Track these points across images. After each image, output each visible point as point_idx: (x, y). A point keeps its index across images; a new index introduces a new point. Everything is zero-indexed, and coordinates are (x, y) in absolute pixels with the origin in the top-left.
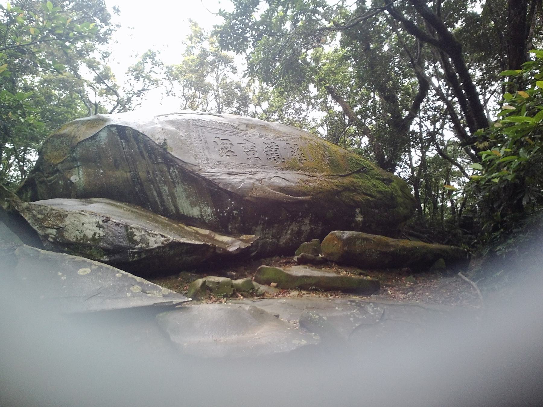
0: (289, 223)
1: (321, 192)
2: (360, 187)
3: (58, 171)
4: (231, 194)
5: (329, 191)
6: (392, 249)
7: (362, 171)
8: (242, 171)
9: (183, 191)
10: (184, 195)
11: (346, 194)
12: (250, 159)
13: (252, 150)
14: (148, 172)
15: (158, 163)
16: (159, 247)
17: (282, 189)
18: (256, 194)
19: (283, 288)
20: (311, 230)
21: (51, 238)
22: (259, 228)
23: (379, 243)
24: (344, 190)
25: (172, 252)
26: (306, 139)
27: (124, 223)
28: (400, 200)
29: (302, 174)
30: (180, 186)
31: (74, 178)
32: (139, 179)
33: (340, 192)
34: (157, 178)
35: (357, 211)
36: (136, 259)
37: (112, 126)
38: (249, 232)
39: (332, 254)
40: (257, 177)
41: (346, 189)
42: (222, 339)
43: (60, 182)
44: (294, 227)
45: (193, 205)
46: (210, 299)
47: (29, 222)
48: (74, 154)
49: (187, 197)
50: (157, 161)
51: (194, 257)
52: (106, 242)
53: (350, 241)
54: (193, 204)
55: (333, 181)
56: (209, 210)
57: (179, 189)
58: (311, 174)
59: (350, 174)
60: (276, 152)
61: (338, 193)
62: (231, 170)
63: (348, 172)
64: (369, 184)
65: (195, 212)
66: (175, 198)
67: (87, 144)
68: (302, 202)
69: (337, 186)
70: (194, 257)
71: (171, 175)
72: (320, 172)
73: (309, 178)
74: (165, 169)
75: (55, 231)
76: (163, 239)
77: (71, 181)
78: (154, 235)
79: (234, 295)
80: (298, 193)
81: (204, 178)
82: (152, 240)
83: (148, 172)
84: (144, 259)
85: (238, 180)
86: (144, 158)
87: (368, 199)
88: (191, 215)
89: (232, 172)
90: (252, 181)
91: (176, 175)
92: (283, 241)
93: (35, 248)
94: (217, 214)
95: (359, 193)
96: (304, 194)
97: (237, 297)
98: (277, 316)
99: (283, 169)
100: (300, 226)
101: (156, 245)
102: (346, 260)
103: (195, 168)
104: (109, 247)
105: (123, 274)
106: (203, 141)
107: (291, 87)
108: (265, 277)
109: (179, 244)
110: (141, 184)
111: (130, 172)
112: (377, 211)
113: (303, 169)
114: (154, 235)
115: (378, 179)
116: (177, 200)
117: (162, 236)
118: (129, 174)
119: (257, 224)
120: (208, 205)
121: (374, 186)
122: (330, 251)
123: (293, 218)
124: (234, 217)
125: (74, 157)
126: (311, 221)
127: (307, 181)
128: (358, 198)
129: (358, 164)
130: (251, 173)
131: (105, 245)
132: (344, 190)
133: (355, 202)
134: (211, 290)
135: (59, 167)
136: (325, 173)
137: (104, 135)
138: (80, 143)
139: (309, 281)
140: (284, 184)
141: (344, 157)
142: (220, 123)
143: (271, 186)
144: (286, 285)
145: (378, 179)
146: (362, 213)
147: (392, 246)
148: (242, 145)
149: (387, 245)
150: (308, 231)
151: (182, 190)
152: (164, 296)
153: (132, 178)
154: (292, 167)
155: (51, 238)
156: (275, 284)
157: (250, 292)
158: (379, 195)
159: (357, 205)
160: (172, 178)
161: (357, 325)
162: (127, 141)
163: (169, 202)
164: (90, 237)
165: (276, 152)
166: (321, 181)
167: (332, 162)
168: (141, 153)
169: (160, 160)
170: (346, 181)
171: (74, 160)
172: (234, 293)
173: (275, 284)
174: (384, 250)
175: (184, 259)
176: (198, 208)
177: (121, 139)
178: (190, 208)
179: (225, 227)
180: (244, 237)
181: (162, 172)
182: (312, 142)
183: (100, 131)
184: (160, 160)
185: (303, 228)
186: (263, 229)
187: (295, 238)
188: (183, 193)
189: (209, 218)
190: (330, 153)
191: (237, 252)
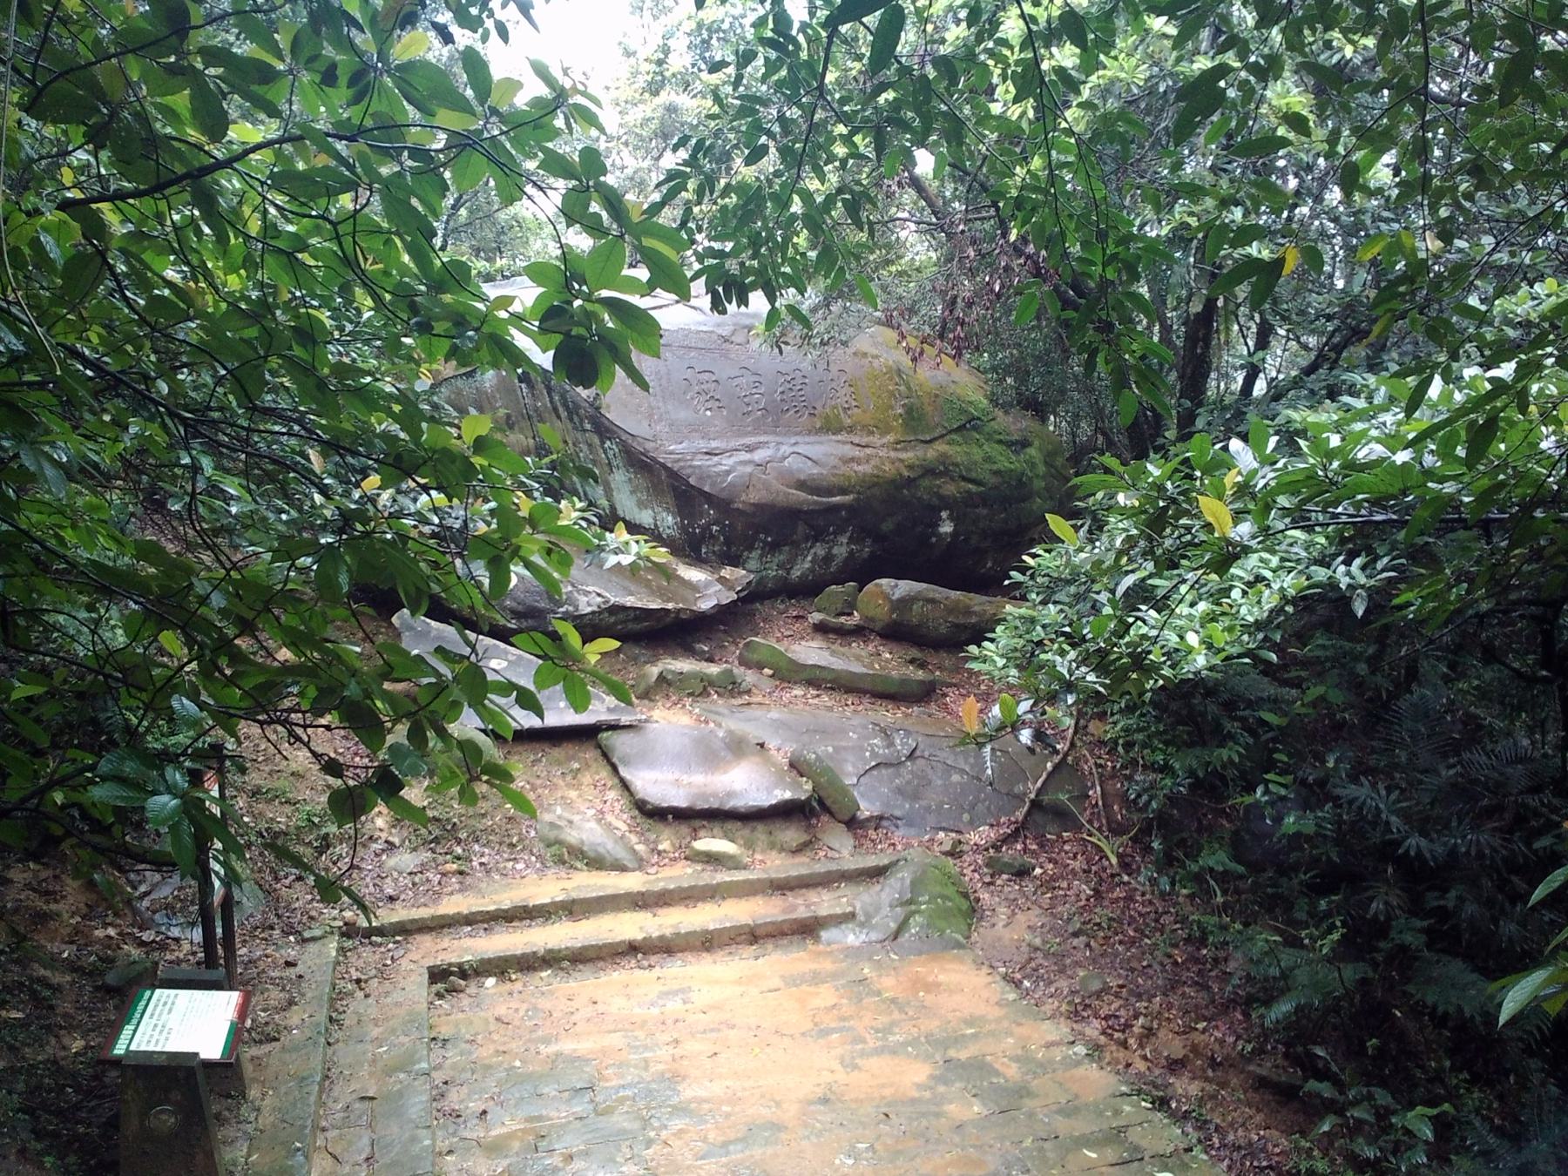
1: (875, 485)
2: (957, 465)
4: (708, 497)
5: (893, 481)
6: (974, 620)
7: (969, 425)
8: (734, 444)
10: (627, 488)
11: (925, 482)
12: (749, 413)
15: (585, 431)
16: (593, 613)
17: (802, 485)
18: (754, 497)
19: (782, 680)
20: (851, 553)
22: (755, 554)
23: (953, 609)
24: (922, 476)
25: (612, 620)
26: (865, 355)
28: (1039, 484)
29: (844, 443)
33: (915, 479)
35: (944, 514)
38: (735, 562)
39: (872, 620)
40: (759, 455)
41: (929, 471)
42: (685, 779)
44: (820, 550)
46: (668, 697)
49: (632, 492)
52: (514, 599)
53: (905, 603)
54: (642, 505)
55: (903, 455)
58: (865, 440)
59: (942, 436)
61: (910, 482)
62: (714, 444)
63: (939, 431)
64: (977, 454)
68: (836, 508)
69: (910, 467)
71: (605, 452)
72: (883, 434)
73: (857, 452)
74: (596, 440)
76: (599, 599)
78: (587, 593)
79: (704, 693)
80: (830, 492)
81: (663, 466)
82: (583, 600)
86: (559, 417)
87: (968, 492)
90: (749, 469)
92: (796, 573)
94: (683, 528)
95: (952, 479)
96: (843, 491)
97: (709, 695)
98: (762, 745)
99: (810, 433)
100: (830, 548)
101: (589, 609)
102: (896, 632)
103: (649, 446)
104: (520, 608)
106: (664, 382)
108: (755, 657)
109: (624, 608)
112: (985, 512)
113: (851, 430)
114: (587, 593)
115: (1000, 442)
119: (751, 548)
120: (667, 510)
121: (988, 459)
122: (871, 614)
123: (818, 536)
124: (712, 536)
126: (850, 538)
127: (852, 460)
128: (950, 489)
129: (963, 411)
131: (514, 604)
132: (922, 476)
133: (941, 498)
134: (669, 684)
136: (890, 438)
139: (825, 674)
140: (810, 471)
141: (937, 396)
142: (698, 332)
143: (783, 475)
144: (790, 674)
145: (1000, 442)
146: (951, 518)
147: (975, 613)
148: (736, 382)
154: (831, 426)
156: (770, 672)
157: (730, 687)
158: (993, 480)
159: (946, 502)
162: (531, 386)
166: (875, 456)
167: (909, 410)
168: (555, 409)
169: (588, 427)
170: (931, 453)
172: (702, 689)
173: (770, 672)
174: (961, 620)
177: (521, 381)
178: (636, 510)
179: (697, 550)
180: (727, 572)
181: (590, 445)
182: (876, 363)
185: (835, 551)
186: (761, 556)
190: (909, 388)
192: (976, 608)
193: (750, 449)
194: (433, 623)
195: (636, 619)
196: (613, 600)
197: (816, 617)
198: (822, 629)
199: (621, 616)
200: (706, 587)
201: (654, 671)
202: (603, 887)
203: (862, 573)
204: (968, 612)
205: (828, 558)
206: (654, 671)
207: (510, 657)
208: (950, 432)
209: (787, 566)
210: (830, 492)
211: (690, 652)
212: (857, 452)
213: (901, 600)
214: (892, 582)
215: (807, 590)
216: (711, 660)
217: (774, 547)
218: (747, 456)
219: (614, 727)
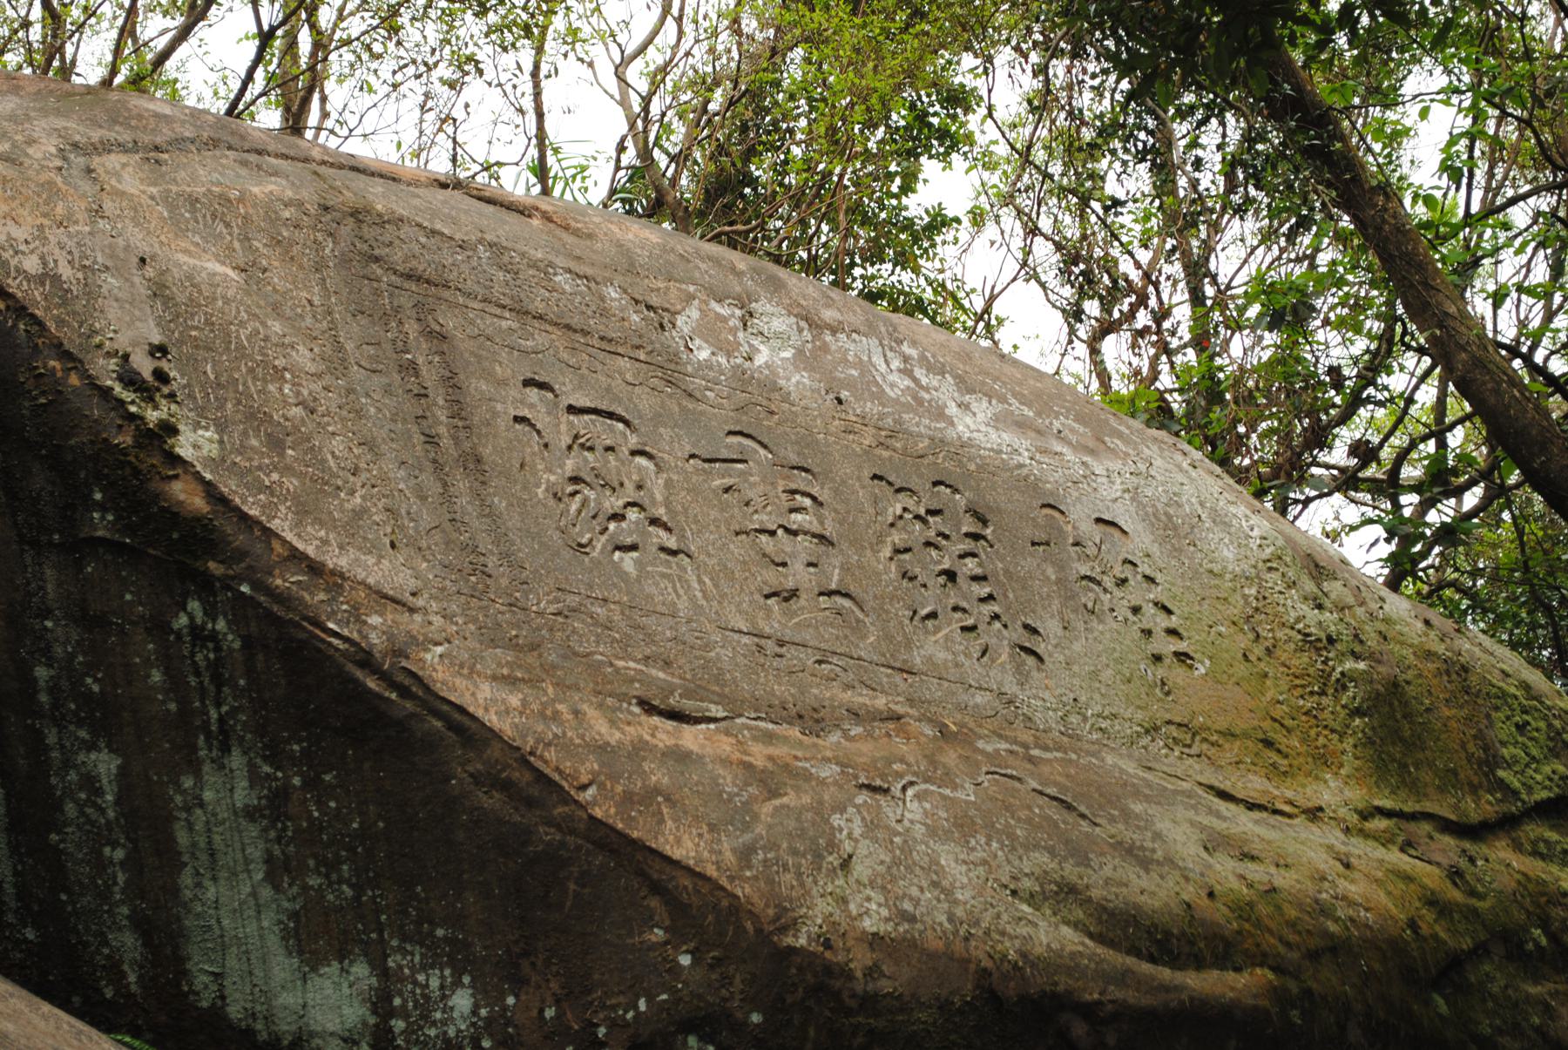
9: (251, 814)
10: (254, 844)
15: (79, 548)
27: (1037, 871)
30: (236, 760)
34: (42, 673)
45: (316, 938)
49: (277, 870)
56: (462, 1001)
57: (224, 790)
61: (1451, 970)
66: (170, 859)
88: (286, 1027)
91: (215, 668)
96: (404, 692)
107: (1249, 200)
116: (186, 878)
149: (1178, 988)
151: (242, 795)
160: (175, 683)
163: (104, 895)
176: (360, 970)
178: (282, 966)
188: (253, 831)
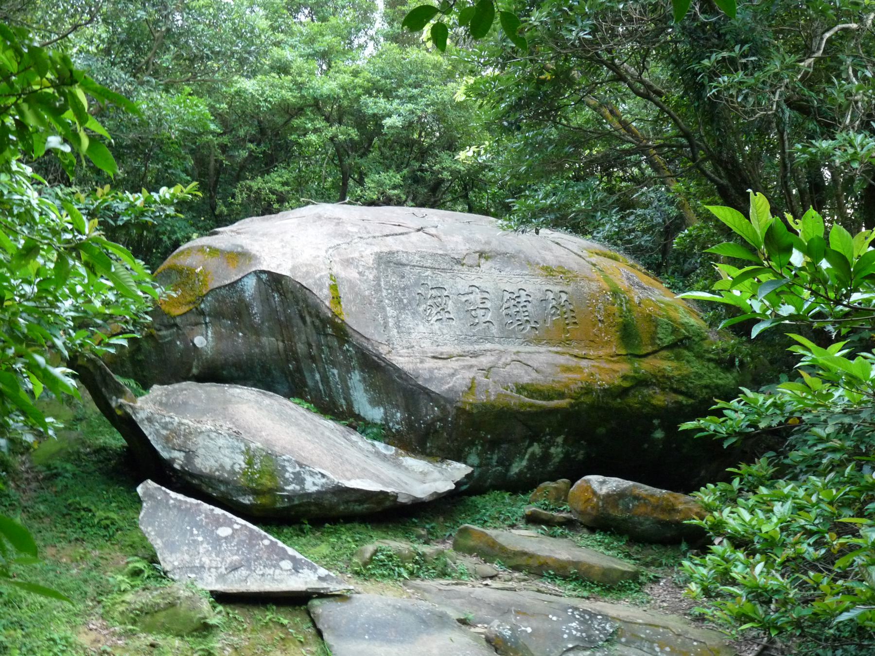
0: (527, 443)
3: (176, 325)
13: (482, 306)
14: (310, 346)
15: (326, 335)
16: (318, 492)
17: (521, 389)
21: (179, 464)
29: (563, 354)
31: (199, 341)
32: (295, 353)
36: (286, 505)
37: (264, 272)
40: (485, 361)
41: (642, 382)
43: (178, 343)
47: (149, 438)
48: (203, 306)
50: (324, 331)
51: (366, 506)
56: (399, 415)
57: (356, 377)
60: (525, 309)
62: (477, 347)
65: (376, 414)
67: (224, 292)
69: (625, 378)
70: (366, 506)
73: (573, 362)
75: (183, 454)
77: (194, 345)
83: (310, 346)
84: (296, 505)
85: (447, 371)
86: (304, 322)
89: (442, 354)
92: (515, 469)
93: (163, 488)
96: (561, 395)
101: (314, 489)
102: (602, 523)
105: (271, 541)
110: (297, 360)
111: (283, 341)
115: (710, 360)
117: (323, 476)
118: (281, 344)
119: (472, 444)
124: (436, 431)
125: (202, 309)
130: (475, 355)
135: (178, 320)
137: (251, 284)
138: (212, 290)
140: (526, 377)
145: (710, 360)
150: (561, 456)
152: (320, 578)
153: (285, 351)
155: (179, 464)
161: (570, 646)
164: (228, 468)
165: (525, 309)
166: (600, 368)
169: (330, 331)
171: (202, 313)
175: (351, 508)
176: (382, 410)
181: (329, 347)
183: (243, 277)
184: (330, 331)
187: (537, 465)
189: (397, 427)
191: (431, 499)
192: (680, 507)
193: (475, 355)
194: (173, 494)
195: (360, 502)
196: (336, 481)
197: (528, 509)
198: (532, 520)
199: (346, 496)
200: (425, 478)
201: (369, 548)
202: (282, 416)
203: (574, 471)
204: (672, 509)
205: (546, 457)
206: (369, 548)
207: (236, 526)
208: (663, 349)
209: (505, 462)
210: (550, 398)
211: (406, 534)
212: (573, 362)
213: (608, 496)
214: (601, 478)
215: (521, 486)
216: (426, 543)
217: (494, 444)
218: (473, 361)
219: (322, 595)
